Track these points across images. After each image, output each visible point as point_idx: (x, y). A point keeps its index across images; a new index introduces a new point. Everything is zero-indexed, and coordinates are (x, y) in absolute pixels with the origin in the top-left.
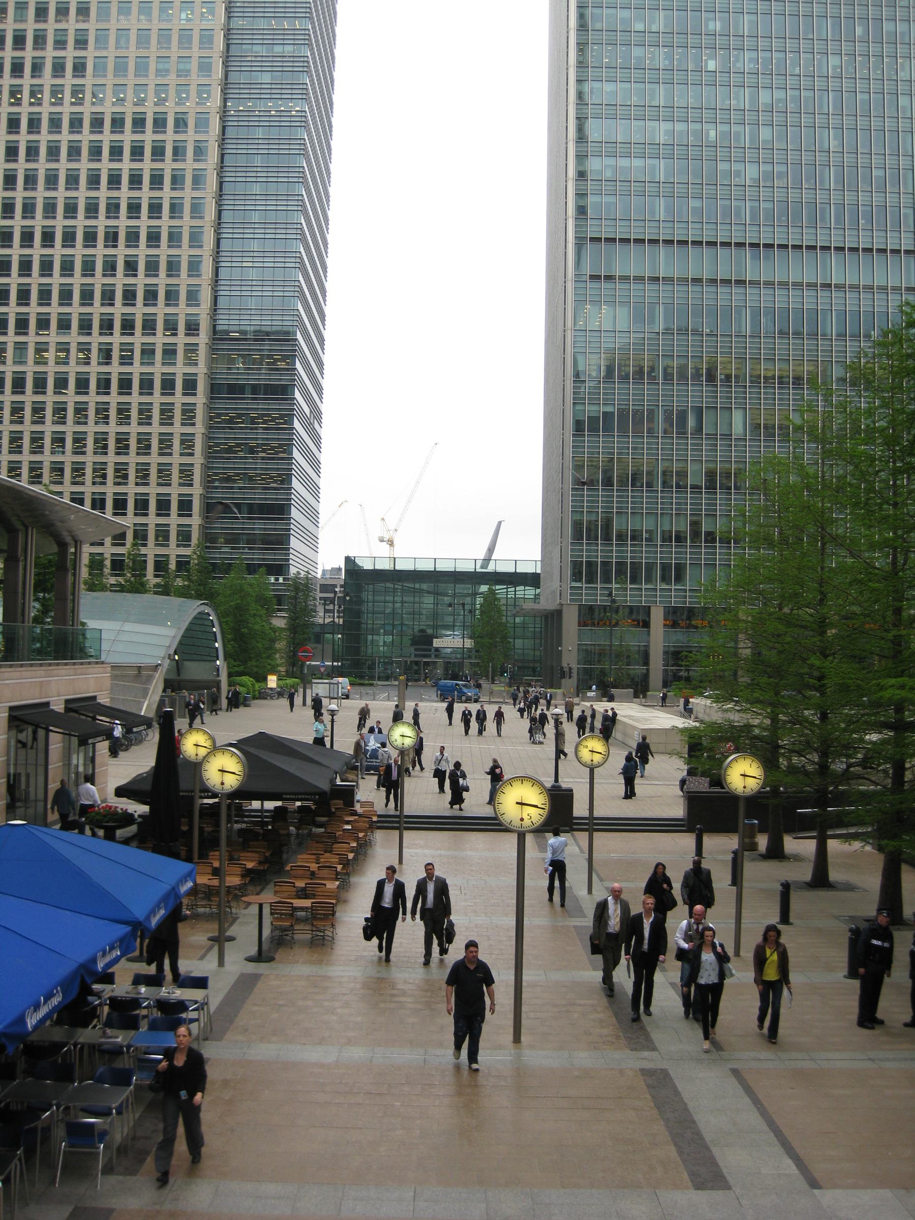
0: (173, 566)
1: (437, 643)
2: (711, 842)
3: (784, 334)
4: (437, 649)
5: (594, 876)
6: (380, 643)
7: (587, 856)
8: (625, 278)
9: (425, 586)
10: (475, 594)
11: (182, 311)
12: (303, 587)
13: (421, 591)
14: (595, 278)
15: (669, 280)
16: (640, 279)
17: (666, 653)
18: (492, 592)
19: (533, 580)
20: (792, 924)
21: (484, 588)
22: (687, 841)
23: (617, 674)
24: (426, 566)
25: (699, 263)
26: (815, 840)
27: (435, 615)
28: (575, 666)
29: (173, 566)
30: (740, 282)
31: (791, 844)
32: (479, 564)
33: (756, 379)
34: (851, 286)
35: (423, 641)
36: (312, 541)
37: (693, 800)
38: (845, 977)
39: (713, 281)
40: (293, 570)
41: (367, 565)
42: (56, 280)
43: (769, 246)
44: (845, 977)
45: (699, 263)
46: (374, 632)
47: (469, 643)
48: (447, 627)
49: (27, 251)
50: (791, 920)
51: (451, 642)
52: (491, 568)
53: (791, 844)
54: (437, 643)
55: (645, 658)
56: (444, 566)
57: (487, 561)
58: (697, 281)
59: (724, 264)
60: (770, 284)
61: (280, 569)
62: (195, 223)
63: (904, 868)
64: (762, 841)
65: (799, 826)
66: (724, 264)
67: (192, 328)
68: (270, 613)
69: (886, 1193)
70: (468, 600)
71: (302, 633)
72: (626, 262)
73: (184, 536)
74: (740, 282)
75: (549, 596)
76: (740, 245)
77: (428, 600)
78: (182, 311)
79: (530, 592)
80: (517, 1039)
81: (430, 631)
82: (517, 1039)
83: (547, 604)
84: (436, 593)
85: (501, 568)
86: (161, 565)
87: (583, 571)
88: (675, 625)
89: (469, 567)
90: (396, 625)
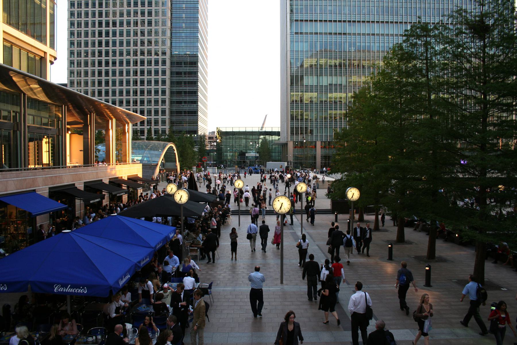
0: (160, 132)
1: (247, 155)
2: (340, 216)
3: (359, 51)
4: (247, 157)
5: (303, 229)
6: (229, 155)
7: (300, 222)
8: (306, 33)
9: (242, 136)
10: (259, 139)
11: (160, 48)
12: (203, 137)
13: (241, 138)
14: (297, 33)
15: (321, 34)
16: (311, 33)
17: (321, 156)
18: (265, 138)
19: (278, 134)
20: (431, 286)
21: (262, 137)
22: (332, 217)
23: (305, 162)
24: (243, 130)
25: (331, 28)
26: (294, 217)
27: (246, 146)
28: (292, 161)
29: (160, 132)
30: (345, 34)
31: (366, 217)
32: (260, 128)
33: (350, 65)
34: (381, 34)
35: (242, 154)
36: (205, 122)
37: (333, 203)
38: (424, 286)
39: (335, 34)
40: (199, 133)
41: (224, 130)
42: (118, 38)
43: (354, 21)
44: (424, 286)
45: (331, 28)
46: (226, 152)
47: (258, 155)
48: (250, 150)
49: (107, 29)
50: (431, 284)
51: (252, 154)
52: (264, 130)
53: (366, 217)
54: (247, 155)
55: (315, 157)
56: (249, 130)
57: (262, 127)
58: (330, 34)
59: (339, 28)
60: (354, 34)
61: (196, 132)
62: (163, 18)
63: (473, 316)
64: (357, 216)
65: (369, 211)
66: (339, 28)
67: (164, 53)
68: (193, 147)
69: (408, 330)
70: (257, 140)
71: (203, 152)
72: (307, 28)
73: (164, 122)
74: (345, 34)
75: (282, 139)
76: (344, 21)
77: (244, 141)
78: (160, 48)
79: (277, 138)
80: (282, 282)
81: (244, 151)
82: (282, 282)
83: (283, 141)
84: (246, 139)
85: (267, 130)
86: (156, 132)
87: (294, 131)
88: (325, 147)
89: (256, 130)
90: (240, 151)
